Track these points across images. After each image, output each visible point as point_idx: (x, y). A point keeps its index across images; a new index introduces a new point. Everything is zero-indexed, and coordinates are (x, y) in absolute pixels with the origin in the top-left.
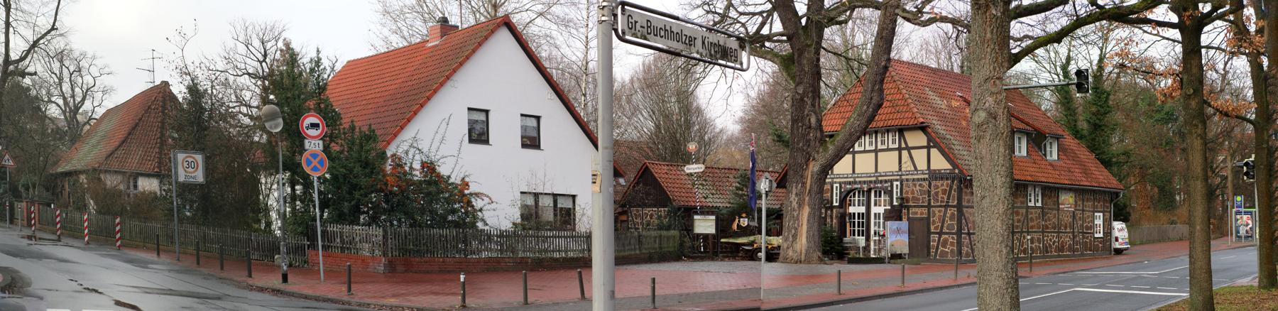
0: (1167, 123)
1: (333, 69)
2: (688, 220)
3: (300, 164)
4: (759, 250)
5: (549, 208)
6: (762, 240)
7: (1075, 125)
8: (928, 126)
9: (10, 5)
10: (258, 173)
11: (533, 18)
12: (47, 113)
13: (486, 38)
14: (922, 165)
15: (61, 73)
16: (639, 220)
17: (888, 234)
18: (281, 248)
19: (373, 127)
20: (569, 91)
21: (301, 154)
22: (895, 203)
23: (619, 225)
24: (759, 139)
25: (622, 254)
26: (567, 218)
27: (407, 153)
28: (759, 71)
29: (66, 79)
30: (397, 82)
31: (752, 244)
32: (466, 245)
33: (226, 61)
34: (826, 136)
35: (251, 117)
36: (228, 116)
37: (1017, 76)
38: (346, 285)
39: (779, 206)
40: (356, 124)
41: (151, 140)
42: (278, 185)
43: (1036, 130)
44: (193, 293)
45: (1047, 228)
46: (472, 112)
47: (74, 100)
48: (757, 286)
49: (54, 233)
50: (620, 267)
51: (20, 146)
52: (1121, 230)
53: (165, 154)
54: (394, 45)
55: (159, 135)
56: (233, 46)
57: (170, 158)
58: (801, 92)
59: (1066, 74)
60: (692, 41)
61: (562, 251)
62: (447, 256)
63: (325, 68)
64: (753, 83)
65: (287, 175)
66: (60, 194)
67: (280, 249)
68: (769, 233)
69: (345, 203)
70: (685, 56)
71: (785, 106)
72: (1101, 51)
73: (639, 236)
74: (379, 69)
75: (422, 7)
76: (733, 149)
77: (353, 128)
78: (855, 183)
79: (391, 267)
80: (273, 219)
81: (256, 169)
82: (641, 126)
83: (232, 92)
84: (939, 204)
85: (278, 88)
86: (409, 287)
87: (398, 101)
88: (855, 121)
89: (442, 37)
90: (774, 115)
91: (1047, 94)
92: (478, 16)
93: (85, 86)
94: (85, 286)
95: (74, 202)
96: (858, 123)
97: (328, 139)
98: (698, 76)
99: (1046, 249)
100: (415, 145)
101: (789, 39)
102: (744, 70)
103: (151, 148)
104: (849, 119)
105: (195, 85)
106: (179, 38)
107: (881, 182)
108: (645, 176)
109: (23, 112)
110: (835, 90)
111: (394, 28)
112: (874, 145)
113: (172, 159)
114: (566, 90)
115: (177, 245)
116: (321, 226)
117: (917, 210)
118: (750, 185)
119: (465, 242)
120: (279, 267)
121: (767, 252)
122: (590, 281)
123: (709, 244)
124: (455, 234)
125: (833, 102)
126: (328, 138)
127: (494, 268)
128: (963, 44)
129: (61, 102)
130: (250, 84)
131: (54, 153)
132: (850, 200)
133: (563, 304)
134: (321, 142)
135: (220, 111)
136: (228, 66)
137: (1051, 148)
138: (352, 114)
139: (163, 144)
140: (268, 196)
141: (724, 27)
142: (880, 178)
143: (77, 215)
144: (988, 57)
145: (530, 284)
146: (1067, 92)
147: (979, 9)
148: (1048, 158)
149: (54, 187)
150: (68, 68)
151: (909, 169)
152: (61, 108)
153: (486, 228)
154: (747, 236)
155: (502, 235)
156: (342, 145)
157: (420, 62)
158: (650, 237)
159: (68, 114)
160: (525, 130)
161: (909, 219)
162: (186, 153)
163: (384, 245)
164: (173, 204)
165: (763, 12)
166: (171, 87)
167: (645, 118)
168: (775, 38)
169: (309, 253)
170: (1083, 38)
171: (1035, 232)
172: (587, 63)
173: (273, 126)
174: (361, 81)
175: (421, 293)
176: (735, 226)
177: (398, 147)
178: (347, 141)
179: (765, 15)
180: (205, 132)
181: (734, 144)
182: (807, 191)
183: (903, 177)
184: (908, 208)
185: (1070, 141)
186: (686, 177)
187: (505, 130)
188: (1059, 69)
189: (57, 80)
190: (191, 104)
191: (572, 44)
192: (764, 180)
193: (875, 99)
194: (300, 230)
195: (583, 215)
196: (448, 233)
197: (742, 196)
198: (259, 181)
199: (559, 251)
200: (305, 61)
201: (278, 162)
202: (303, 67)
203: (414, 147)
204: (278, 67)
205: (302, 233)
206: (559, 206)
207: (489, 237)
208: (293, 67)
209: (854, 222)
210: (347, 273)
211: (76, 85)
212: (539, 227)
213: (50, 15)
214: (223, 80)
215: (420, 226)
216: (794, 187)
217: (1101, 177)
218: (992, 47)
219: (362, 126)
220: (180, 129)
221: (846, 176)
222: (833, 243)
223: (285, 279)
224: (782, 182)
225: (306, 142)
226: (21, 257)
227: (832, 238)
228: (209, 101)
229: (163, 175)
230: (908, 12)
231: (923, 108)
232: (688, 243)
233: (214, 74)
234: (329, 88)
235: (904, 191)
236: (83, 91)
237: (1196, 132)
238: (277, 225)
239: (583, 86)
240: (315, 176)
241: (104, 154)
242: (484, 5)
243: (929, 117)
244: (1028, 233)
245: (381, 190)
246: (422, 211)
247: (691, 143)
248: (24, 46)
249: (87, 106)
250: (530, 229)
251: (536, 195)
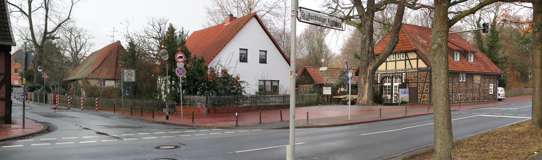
0: (526, 44)
3: (174, 73)
4: (348, 100)
5: (269, 86)
6: (349, 97)
7: (482, 47)
8: (417, 50)
9: (48, 8)
10: (157, 77)
13: (247, 22)
14: (415, 66)
15: (71, 37)
17: (400, 93)
18: (166, 106)
19: (203, 57)
21: (175, 68)
22: (403, 82)
24: (348, 57)
25: (297, 103)
27: (216, 67)
31: (345, 98)
32: (238, 102)
34: (376, 55)
35: (154, 55)
36: (145, 54)
37: (456, 27)
38: (192, 119)
39: (356, 83)
40: (197, 56)
41: (112, 65)
43: (464, 50)
45: (468, 90)
48: (347, 115)
49: (66, 106)
52: (502, 91)
55: (115, 63)
56: (147, 26)
59: (478, 25)
61: (274, 102)
62: (231, 106)
64: (346, 35)
68: (352, 94)
71: (359, 43)
72: (495, 14)
77: (195, 58)
78: (387, 74)
79: (209, 111)
81: (156, 76)
82: (304, 53)
84: (422, 81)
87: (213, 47)
88: (387, 49)
89: (230, 21)
90: (354, 47)
91: (470, 34)
94: (83, 127)
95: (75, 93)
96: (389, 50)
97: (186, 62)
99: (467, 99)
100: (219, 63)
101: (360, 17)
104: (385, 48)
107: (397, 73)
108: (305, 72)
110: (378, 36)
112: (400, 58)
113: (122, 72)
114: (276, 41)
115: (123, 107)
117: (412, 84)
120: (165, 113)
121: (351, 102)
125: (378, 41)
127: (248, 110)
128: (432, 16)
129: (70, 50)
132: (385, 81)
133: (275, 123)
137: (470, 57)
140: (161, 85)
142: (397, 72)
143: (78, 98)
144: (438, 22)
145: (262, 116)
146: (479, 33)
147: (438, 4)
148: (469, 61)
150: (74, 35)
151: (409, 68)
158: (307, 96)
160: (261, 57)
161: (409, 88)
162: (128, 70)
163: (206, 103)
168: (355, 17)
169: (177, 107)
170: (487, 10)
171: (462, 92)
172: (285, 30)
176: (339, 91)
179: (351, 8)
182: (368, 77)
183: (407, 71)
184: (409, 83)
185: (479, 54)
186: (320, 72)
187: (253, 57)
188: (475, 23)
190: (130, 50)
191: (279, 23)
192: (350, 72)
193: (396, 40)
194: (173, 98)
196: (231, 97)
200: (177, 33)
201: (166, 72)
203: (219, 64)
205: (174, 100)
206: (273, 85)
207: (247, 98)
209: (386, 89)
210: (192, 115)
211: (77, 43)
212: (265, 93)
213: (67, 13)
215: (220, 95)
216: (362, 76)
217: (493, 68)
218: (440, 18)
219: (199, 57)
220: (125, 60)
221: (383, 71)
222: (378, 98)
223: (167, 118)
224: (357, 74)
225: (177, 63)
226: (51, 117)
227: (377, 95)
230: (409, 4)
231: (415, 43)
232: (321, 98)
233: (140, 38)
234: (186, 42)
235: (407, 77)
236: (81, 45)
237: (538, 48)
240: (180, 76)
241: (91, 71)
243: (418, 46)
244: (459, 92)
245: (206, 81)
249: (82, 51)
250: (262, 94)
251: (265, 81)
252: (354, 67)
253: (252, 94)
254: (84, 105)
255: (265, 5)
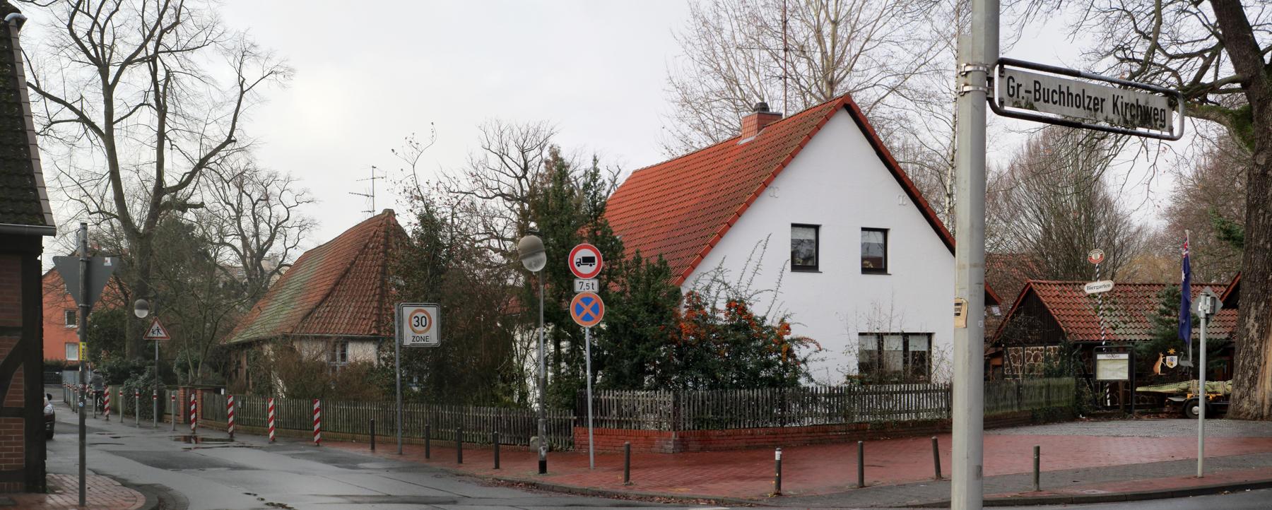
1: (614, 183)
2: (1088, 362)
3: (567, 313)
4: (1195, 402)
5: (896, 353)
6: (1200, 387)
9: (166, 107)
10: (512, 328)
11: (881, 96)
12: (218, 260)
13: (819, 128)
15: (240, 203)
16: (1018, 365)
19: (664, 258)
20: (929, 192)
21: (569, 299)
23: (991, 372)
24: (1196, 238)
26: (920, 365)
27: (708, 289)
28: (1198, 139)
29: (247, 211)
30: (698, 195)
31: (1183, 393)
32: (783, 410)
33: (473, 179)
38: (623, 472)
39: (1226, 336)
42: (538, 342)
44: (420, 497)
46: (796, 229)
47: (258, 241)
49: (224, 430)
50: (991, 432)
51: (176, 309)
53: (386, 309)
54: (696, 145)
55: (378, 284)
56: (482, 157)
57: (393, 314)
58: (1262, 162)
60: (1098, 104)
61: (911, 412)
62: (758, 427)
63: (603, 183)
64: (1189, 155)
65: (550, 328)
66: (234, 373)
67: (537, 429)
68: (1209, 377)
69: (626, 361)
70: (1087, 127)
71: (1238, 185)
73: (1019, 387)
74: (675, 178)
75: (733, 92)
76: (1157, 255)
77: (638, 261)
80: (530, 388)
81: (509, 323)
83: (480, 220)
85: (541, 212)
86: (704, 471)
89: (759, 130)
90: (1221, 200)
92: (808, 98)
93: (274, 221)
95: (254, 384)
97: (605, 277)
98: (1106, 153)
100: (720, 278)
101: (1245, 86)
102: (1172, 139)
103: (367, 302)
105: (430, 213)
106: (409, 149)
108: (1029, 301)
109: (183, 261)
111: (696, 122)
113: (396, 315)
114: (925, 190)
115: (399, 434)
116: (593, 393)
118: (1181, 306)
119: (783, 406)
120: (536, 452)
122: (949, 453)
123: (1118, 395)
124: (769, 396)
126: (605, 276)
127: (820, 439)
129: (238, 243)
130: (504, 208)
131: (226, 316)
134: (596, 282)
135: (462, 247)
136: (476, 186)
138: (637, 242)
139: (383, 294)
141: (1145, 79)
143: (259, 402)
149: (226, 363)
150: (249, 196)
152: (238, 252)
153: (811, 385)
154: (1176, 382)
155: (832, 393)
156: (623, 284)
157: (729, 166)
158: (1034, 387)
159: (248, 260)
160: (868, 249)
164: (394, 376)
165: (1205, 51)
166: (397, 217)
167: (1030, 220)
168: (1223, 87)
169: (576, 431)
173: (533, 263)
174: (650, 197)
175: (722, 479)
176: (1158, 368)
177: (694, 284)
178: (630, 278)
179: (1207, 55)
180: (442, 277)
181: (1157, 247)
186: (1087, 300)
189: (233, 213)
191: (934, 126)
192: (1203, 298)
194: (564, 400)
195: (942, 359)
196: (760, 395)
197: (1169, 322)
198: (512, 339)
199: (908, 412)
200: (577, 174)
201: (538, 311)
202: (574, 183)
203: (718, 281)
204: (542, 184)
205: (567, 405)
206: (911, 349)
207: (815, 397)
208: (562, 184)
210: (625, 457)
211: (261, 219)
214: (467, 204)
215: (722, 387)
219: (650, 257)
220: (407, 273)
223: (543, 468)
224: (1230, 301)
225: (577, 282)
228: (449, 234)
229: (383, 339)
232: (1088, 394)
233: (456, 197)
234: (608, 208)
236: (271, 227)
238: (534, 395)
239: (948, 183)
240: (586, 327)
242: (816, 83)
245: (673, 341)
246: (727, 367)
247: (1095, 251)
248: (187, 167)
249: (277, 247)
250: (870, 383)
251: (880, 337)
252: (1218, 276)
253: (834, 385)
254: (276, 426)
255: (884, 65)
